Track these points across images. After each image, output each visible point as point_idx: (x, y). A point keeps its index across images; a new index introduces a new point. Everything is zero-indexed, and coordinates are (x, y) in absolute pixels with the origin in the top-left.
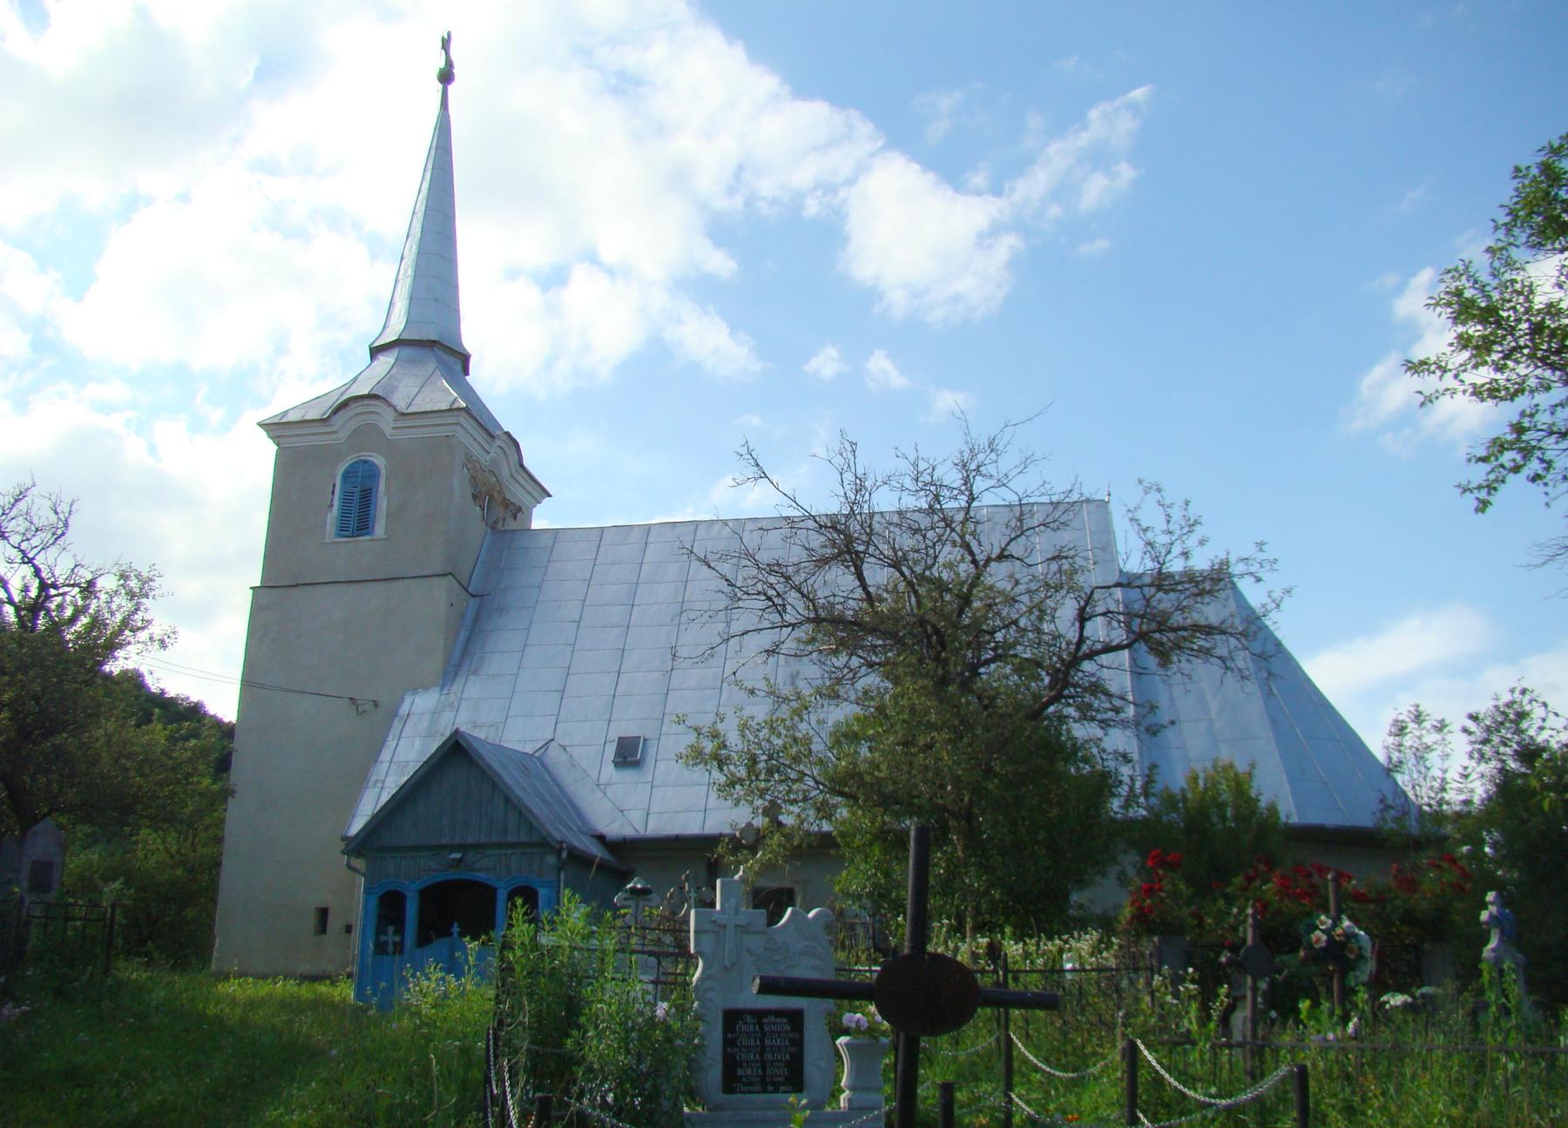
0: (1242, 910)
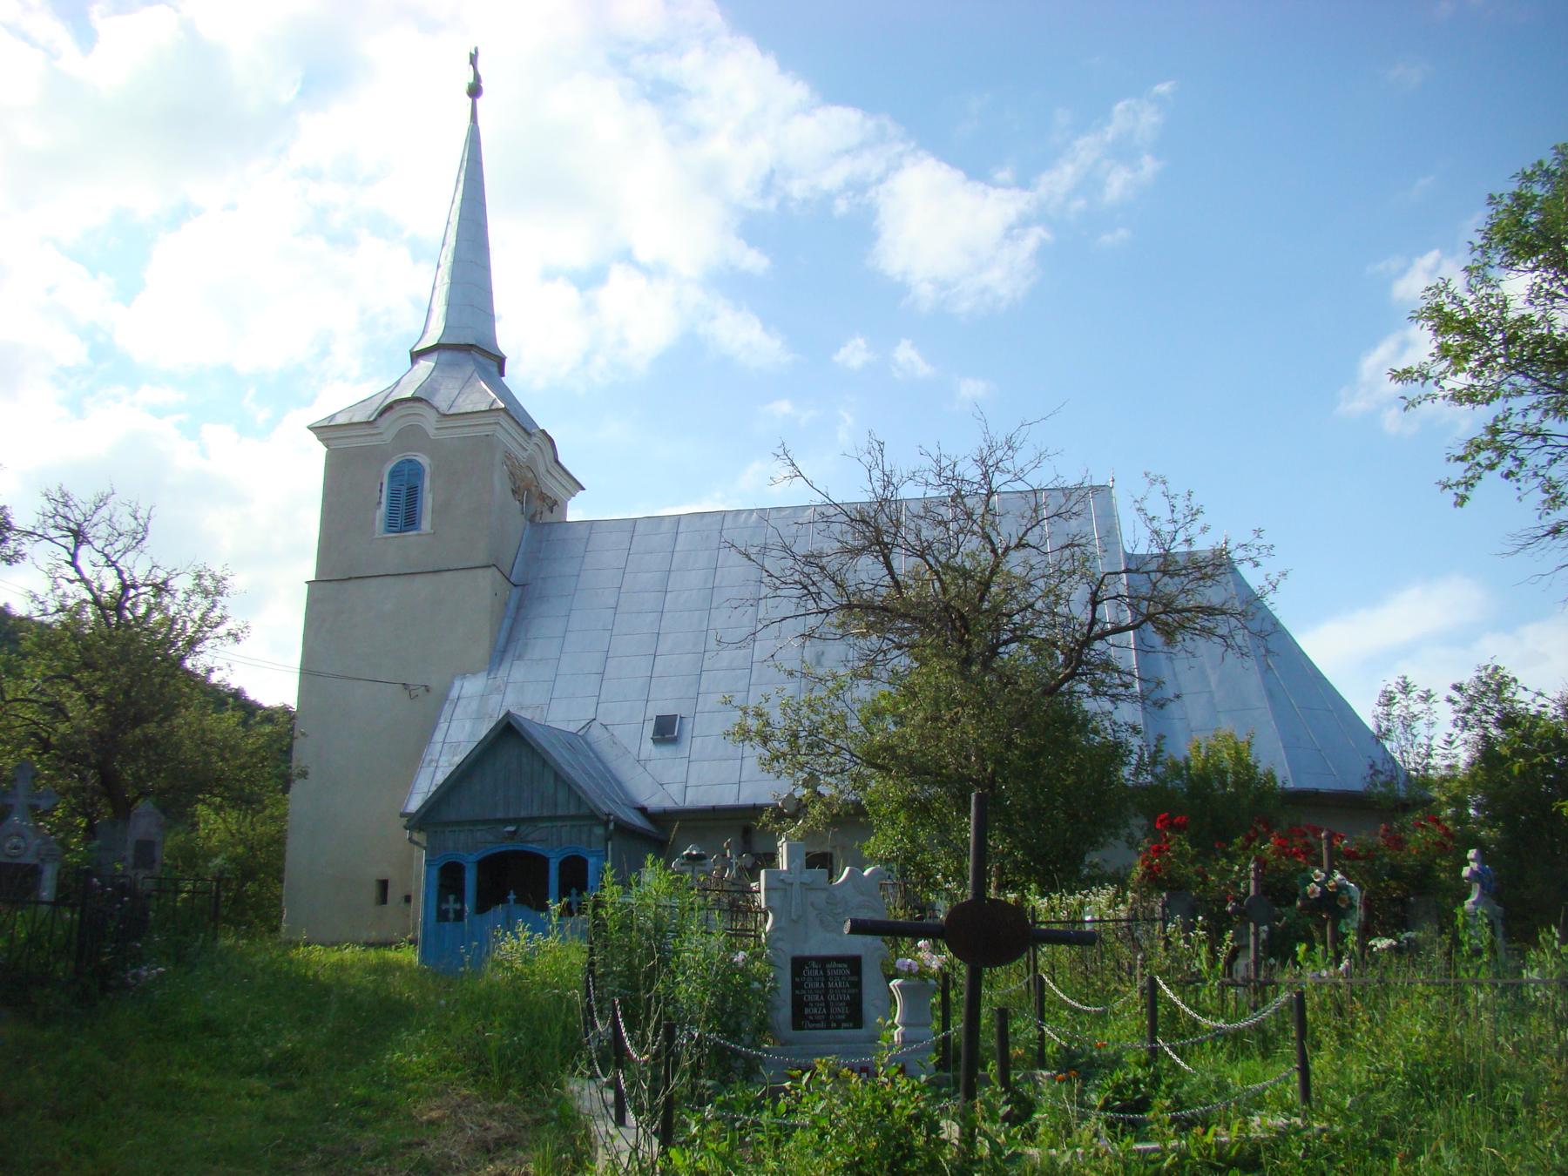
0: (1243, 867)
